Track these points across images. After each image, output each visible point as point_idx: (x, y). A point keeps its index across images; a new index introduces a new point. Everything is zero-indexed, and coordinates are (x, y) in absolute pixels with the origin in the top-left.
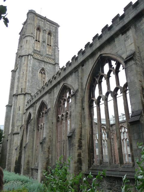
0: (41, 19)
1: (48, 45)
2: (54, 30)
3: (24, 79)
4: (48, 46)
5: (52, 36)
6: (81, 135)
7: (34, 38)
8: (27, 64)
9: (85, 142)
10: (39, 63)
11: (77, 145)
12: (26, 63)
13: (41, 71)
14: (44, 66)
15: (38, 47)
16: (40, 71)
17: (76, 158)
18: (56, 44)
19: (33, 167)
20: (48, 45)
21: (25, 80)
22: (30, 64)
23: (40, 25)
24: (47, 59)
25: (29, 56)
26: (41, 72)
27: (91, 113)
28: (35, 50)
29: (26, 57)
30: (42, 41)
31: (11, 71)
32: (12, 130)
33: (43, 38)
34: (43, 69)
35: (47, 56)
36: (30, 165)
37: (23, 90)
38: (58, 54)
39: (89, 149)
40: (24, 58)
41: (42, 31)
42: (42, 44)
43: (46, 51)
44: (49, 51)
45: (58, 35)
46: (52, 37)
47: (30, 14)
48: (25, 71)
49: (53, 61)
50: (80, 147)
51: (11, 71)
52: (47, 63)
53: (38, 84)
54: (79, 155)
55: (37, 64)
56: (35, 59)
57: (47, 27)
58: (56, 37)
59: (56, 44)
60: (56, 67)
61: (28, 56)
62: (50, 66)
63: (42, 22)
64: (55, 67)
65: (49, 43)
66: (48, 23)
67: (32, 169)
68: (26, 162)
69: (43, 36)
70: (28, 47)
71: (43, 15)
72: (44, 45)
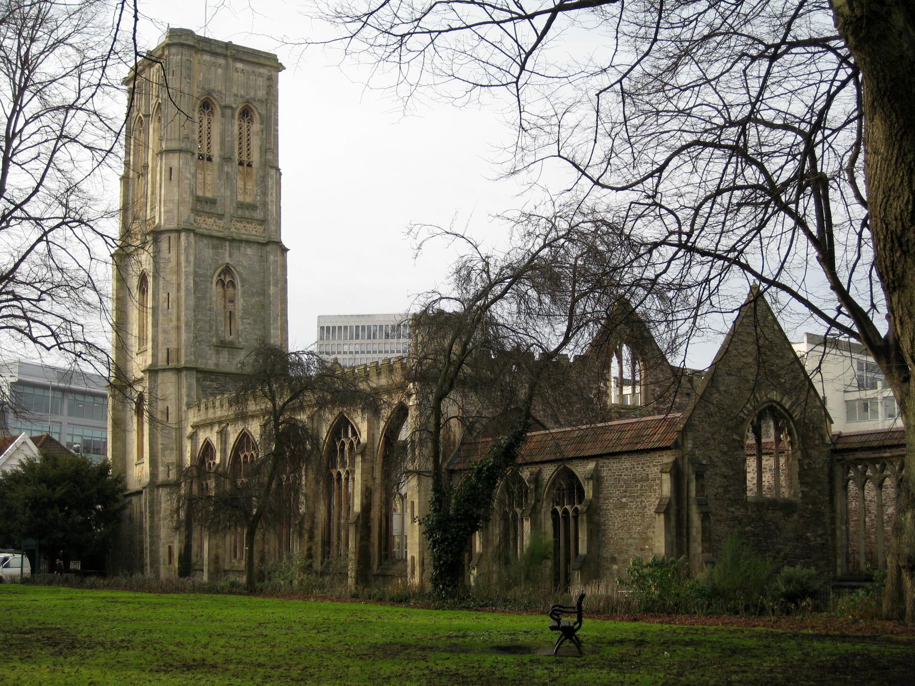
0: (213, 59)
1: (241, 163)
3: (174, 318)
4: (241, 168)
5: (256, 118)
7: (193, 154)
10: (215, 247)
14: (230, 256)
16: (219, 275)
20: (241, 163)
21: (174, 323)
25: (183, 235)
26: (221, 282)
32: (153, 474)
34: (227, 270)
37: (173, 356)
41: (218, 111)
46: (256, 127)
48: (175, 290)
52: (241, 241)
53: (214, 328)
54: (310, 549)
61: (178, 231)
62: (249, 251)
65: (245, 158)
70: (176, 198)
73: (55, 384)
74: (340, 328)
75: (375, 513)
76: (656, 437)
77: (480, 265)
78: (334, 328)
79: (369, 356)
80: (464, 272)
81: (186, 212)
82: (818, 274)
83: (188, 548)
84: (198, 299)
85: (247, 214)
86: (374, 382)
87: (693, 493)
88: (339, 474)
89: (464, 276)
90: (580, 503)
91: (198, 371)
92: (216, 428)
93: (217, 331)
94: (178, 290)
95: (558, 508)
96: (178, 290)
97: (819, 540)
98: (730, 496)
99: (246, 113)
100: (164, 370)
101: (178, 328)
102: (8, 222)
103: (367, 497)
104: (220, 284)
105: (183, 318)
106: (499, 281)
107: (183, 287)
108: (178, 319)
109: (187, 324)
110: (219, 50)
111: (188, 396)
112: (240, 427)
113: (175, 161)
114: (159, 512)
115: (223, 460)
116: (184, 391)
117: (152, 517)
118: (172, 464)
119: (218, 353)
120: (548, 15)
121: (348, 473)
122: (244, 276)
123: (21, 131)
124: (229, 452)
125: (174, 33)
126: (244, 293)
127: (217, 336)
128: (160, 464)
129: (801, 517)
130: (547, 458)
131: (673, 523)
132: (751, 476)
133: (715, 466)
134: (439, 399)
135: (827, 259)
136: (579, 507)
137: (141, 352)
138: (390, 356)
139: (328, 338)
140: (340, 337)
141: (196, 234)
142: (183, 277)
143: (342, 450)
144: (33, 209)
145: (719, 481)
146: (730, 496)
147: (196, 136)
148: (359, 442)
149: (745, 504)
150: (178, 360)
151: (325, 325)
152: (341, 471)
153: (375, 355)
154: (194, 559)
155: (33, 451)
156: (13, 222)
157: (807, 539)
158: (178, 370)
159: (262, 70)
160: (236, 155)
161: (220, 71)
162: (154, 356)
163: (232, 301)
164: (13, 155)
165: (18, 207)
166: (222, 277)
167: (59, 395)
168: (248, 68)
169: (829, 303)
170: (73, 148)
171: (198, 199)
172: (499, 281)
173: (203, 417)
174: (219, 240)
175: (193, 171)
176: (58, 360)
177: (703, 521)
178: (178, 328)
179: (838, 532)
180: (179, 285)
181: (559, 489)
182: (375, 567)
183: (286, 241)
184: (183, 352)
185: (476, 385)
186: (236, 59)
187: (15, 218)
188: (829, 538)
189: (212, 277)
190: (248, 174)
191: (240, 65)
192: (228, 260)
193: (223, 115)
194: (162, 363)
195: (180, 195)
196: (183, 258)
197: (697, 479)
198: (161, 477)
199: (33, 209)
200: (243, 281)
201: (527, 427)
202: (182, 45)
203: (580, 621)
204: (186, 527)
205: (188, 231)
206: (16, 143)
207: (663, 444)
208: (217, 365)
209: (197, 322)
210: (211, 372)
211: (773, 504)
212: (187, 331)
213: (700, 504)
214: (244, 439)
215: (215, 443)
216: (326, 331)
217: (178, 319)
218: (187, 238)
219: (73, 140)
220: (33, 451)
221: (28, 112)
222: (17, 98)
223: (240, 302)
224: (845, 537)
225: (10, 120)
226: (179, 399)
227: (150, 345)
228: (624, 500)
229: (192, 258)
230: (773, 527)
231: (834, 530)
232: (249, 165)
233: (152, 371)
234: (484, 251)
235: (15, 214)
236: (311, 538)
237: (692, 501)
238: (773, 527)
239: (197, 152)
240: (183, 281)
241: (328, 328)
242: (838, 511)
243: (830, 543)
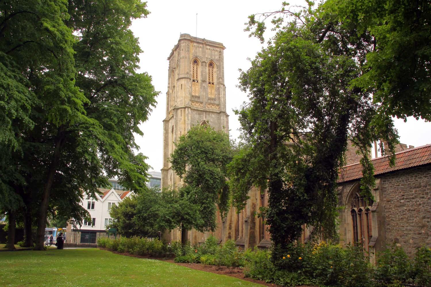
0: (198, 45)
1: (209, 83)
2: (217, 57)
4: (209, 85)
5: (215, 66)
6: (231, 221)
7: (190, 79)
8: (185, 120)
9: (233, 226)
10: (199, 114)
11: (228, 227)
12: (183, 119)
14: (206, 117)
15: (197, 90)
18: (221, 80)
19: (200, 242)
20: (209, 83)
22: (188, 119)
23: (198, 54)
24: (209, 106)
25: (186, 109)
28: (193, 96)
29: (183, 110)
30: (201, 80)
31: (163, 121)
33: (202, 75)
35: (209, 101)
36: (197, 239)
38: (225, 95)
39: (236, 230)
40: (179, 111)
41: (200, 64)
42: (202, 84)
43: (207, 94)
44: (211, 93)
45: (223, 64)
46: (215, 69)
47: (182, 42)
48: (183, 130)
49: (217, 107)
50: (230, 228)
51: (163, 121)
52: (210, 112)
54: (230, 233)
55: (197, 116)
56: (194, 110)
57: (208, 54)
58: (221, 68)
59: (221, 80)
60: (222, 118)
61: (185, 108)
62: (213, 116)
63: (200, 49)
64: (221, 116)
65: (211, 81)
66: (208, 47)
67: (199, 243)
68: (194, 237)
69: (202, 72)
70: (184, 95)
71: (200, 36)
72: (204, 86)
85: (212, 102)
95: (356, 209)
99: (211, 65)
103: (253, 208)
110: (200, 42)
136: (370, 207)
141: (191, 109)
159: (217, 49)
168: (212, 48)
175: (190, 85)
180: (185, 128)
192: (204, 119)
193: (202, 65)
218: (188, 110)
229: (190, 118)
232: (213, 84)
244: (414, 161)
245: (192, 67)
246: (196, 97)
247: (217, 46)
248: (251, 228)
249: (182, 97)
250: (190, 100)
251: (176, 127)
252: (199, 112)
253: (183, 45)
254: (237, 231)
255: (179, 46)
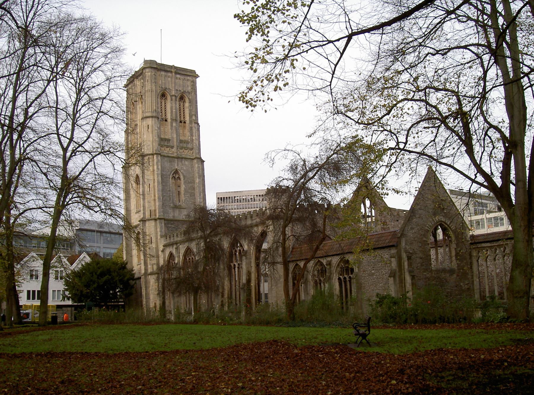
0: (166, 74)
1: (181, 122)
3: (153, 195)
4: (181, 124)
5: (187, 100)
7: (158, 118)
10: (170, 162)
13: (174, 175)
14: (178, 165)
17: (220, 303)
20: (181, 122)
21: (153, 198)
25: (155, 156)
26: (174, 177)
27: (126, 197)
29: (150, 156)
32: (146, 270)
34: (176, 172)
37: (153, 213)
41: (169, 98)
46: (187, 104)
48: (152, 182)
52: (182, 158)
54: (222, 301)
55: (167, 165)
56: (164, 156)
58: (194, 103)
61: (153, 154)
62: (186, 163)
70: (151, 139)
73: (97, 229)
74: (227, 198)
75: (253, 284)
76: (387, 241)
77: (302, 163)
78: (224, 198)
79: (241, 210)
80: (294, 167)
81: (156, 145)
82: (467, 160)
83: (164, 303)
84: (163, 185)
85: (185, 145)
86: (249, 222)
87: (406, 267)
88: (235, 265)
89: (293, 169)
90: (352, 274)
91: (165, 219)
92: (175, 246)
93: (173, 200)
94: (154, 183)
95: (341, 277)
96: (154, 183)
97: (466, 287)
98: (424, 267)
99: (182, 98)
100: (149, 220)
101: (155, 200)
102: (75, 154)
103: (248, 276)
104: (173, 179)
105: (157, 195)
106: (311, 170)
107: (156, 180)
108: (155, 196)
109: (159, 198)
110: (169, 69)
111: (161, 231)
112: (186, 245)
113: (150, 122)
114: (149, 287)
115: (179, 261)
116: (158, 230)
117: (146, 290)
118: (154, 264)
119: (174, 211)
120: (346, 39)
121: (239, 264)
122: (185, 174)
123: (80, 110)
124: (181, 257)
125: (146, 62)
126: (185, 182)
127: (173, 203)
128: (149, 264)
129: (458, 276)
130: (335, 253)
131: (398, 281)
132: (433, 257)
133: (416, 254)
134: (285, 226)
135: (470, 152)
136: (351, 276)
137: (138, 212)
138: (250, 210)
139: (221, 203)
140: (227, 202)
141: (161, 156)
142: (156, 176)
143: (236, 254)
144: (87, 146)
145: (418, 260)
146: (424, 267)
147: (159, 110)
148: (243, 250)
149: (431, 271)
150: (155, 215)
151: (220, 197)
152: (236, 264)
153: (243, 210)
154: (167, 308)
155: (88, 259)
156: (77, 153)
157: (461, 286)
158: (155, 220)
159: (189, 78)
160: (178, 118)
161: (169, 79)
162: (144, 213)
163: (179, 186)
164: (77, 121)
165: (80, 146)
166: (174, 175)
167: (99, 234)
168: (182, 77)
169: (472, 172)
170: (104, 117)
171: (161, 140)
172: (311, 170)
173: (168, 241)
174: (171, 158)
175: (159, 126)
176: (98, 217)
177: (412, 280)
178: (155, 200)
179: (475, 282)
180: (154, 180)
181: (341, 268)
182: (254, 309)
183: (203, 157)
184: (157, 211)
185: (300, 220)
186: (176, 73)
187: (78, 151)
188: (471, 285)
189: (170, 176)
190: (184, 127)
191: (178, 76)
192: (176, 167)
194: (147, 216)
195: (153, 138)
196: (155, 167)
197: (408, 260)
198: (150, 271)
199: (87, 146)
200: (184, 177)
201: (324, 239)
202: (152, 68)
203: (369, 331)
204: (162, 293)
205: (156, 154)
206: (78, 115)
207: (391, 244)
208: (174, 216)
209: (163, 197)
210: (171, 220)
211: (444, 270)
212: (159, 201)
213: (410, 272)
214: (188, 251)
215: (175, 253)
216: (221, 199)
217: (155, 196)
218: (157, 157)
219: (105, 114)
220: (88, 259)
221: (83, 102)
222: (78, 93)
223: (183, 187)
224: (478, 284)
225: (75, 105)
226: (156, 233)
227: (142, 209)
228: (373, 272)
229: (160, 167)
230: (445, 281)
231: (473, 281)
232: (185, 122)
233: (143, 221)
234: (303, 157)
235: (78, 149)
236: (223, 296)
237: (406, 270)
238: (445, 281)
239: (160, 117)
240: (156, 178)
241: (221, 198)
242: (475, 272)
243: (472, 287)
244: (381, 242)
245: (160, 103)
246: (166, 140)
247: (188, 74)
248: (247, 295)
249: (149, 141)
250: (159, 145)
251: (143, 177)
252: (171, 159)
253: (148, 73)
254: (230, 297)
255: (141, 74)
